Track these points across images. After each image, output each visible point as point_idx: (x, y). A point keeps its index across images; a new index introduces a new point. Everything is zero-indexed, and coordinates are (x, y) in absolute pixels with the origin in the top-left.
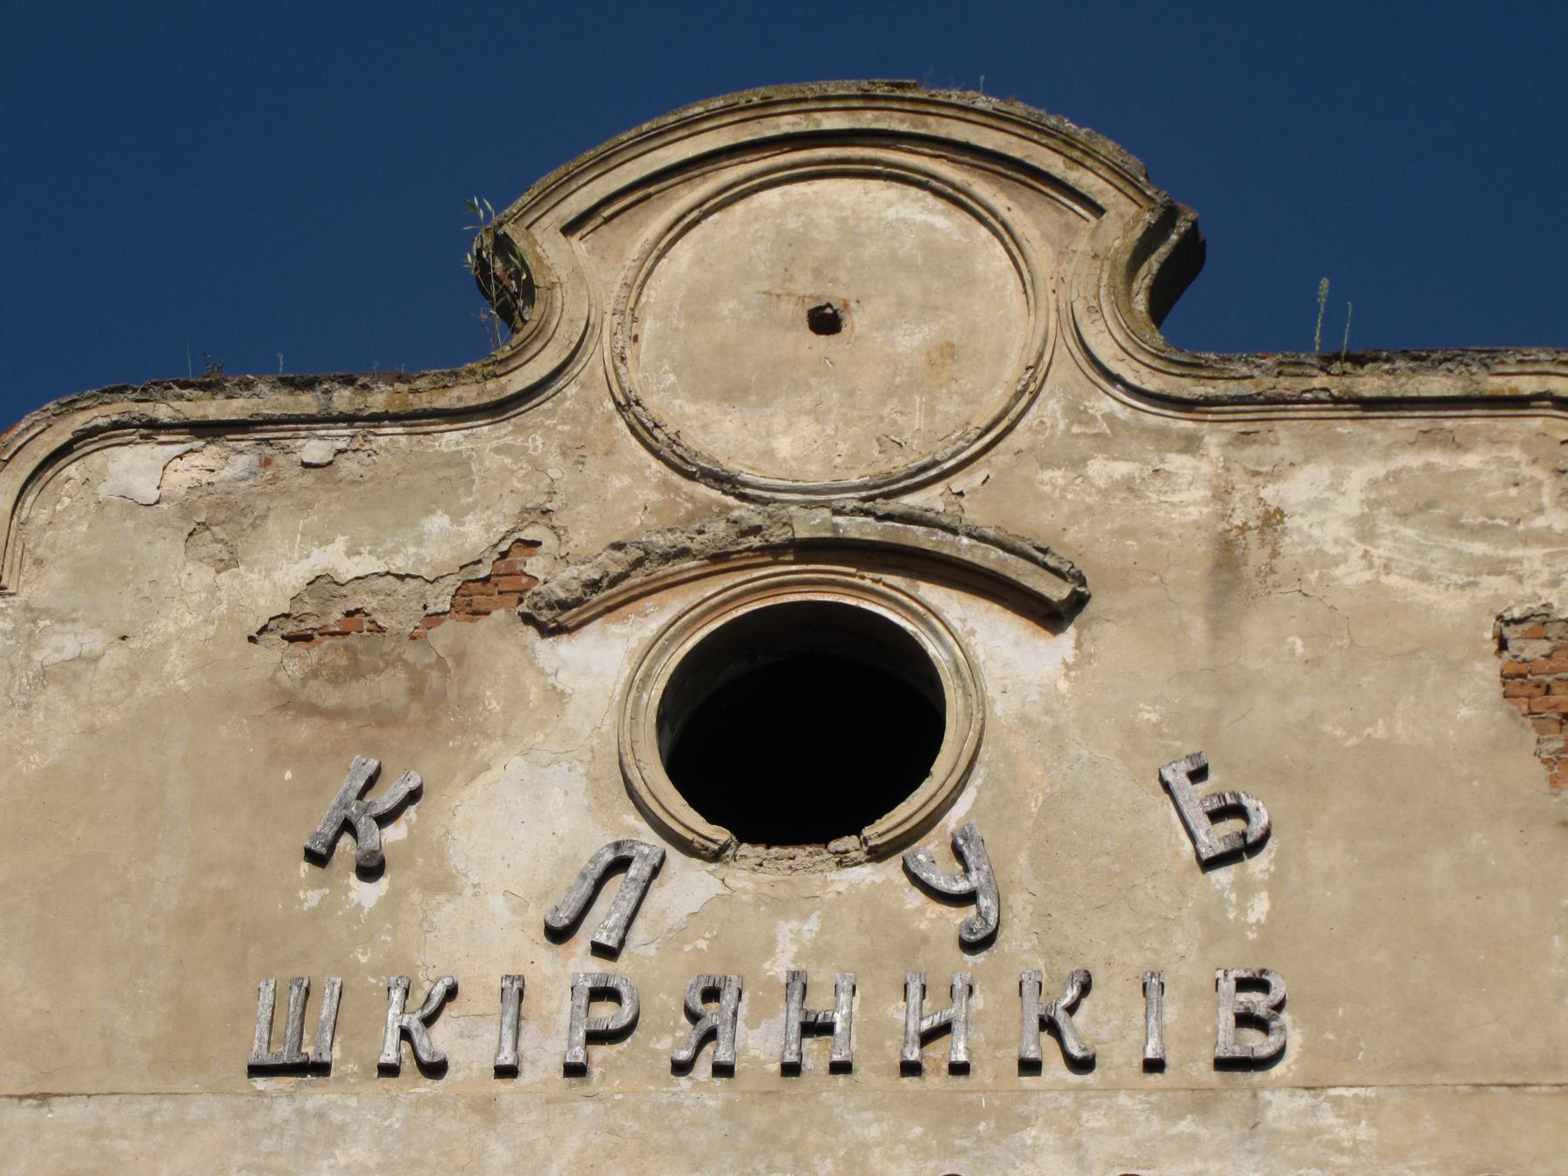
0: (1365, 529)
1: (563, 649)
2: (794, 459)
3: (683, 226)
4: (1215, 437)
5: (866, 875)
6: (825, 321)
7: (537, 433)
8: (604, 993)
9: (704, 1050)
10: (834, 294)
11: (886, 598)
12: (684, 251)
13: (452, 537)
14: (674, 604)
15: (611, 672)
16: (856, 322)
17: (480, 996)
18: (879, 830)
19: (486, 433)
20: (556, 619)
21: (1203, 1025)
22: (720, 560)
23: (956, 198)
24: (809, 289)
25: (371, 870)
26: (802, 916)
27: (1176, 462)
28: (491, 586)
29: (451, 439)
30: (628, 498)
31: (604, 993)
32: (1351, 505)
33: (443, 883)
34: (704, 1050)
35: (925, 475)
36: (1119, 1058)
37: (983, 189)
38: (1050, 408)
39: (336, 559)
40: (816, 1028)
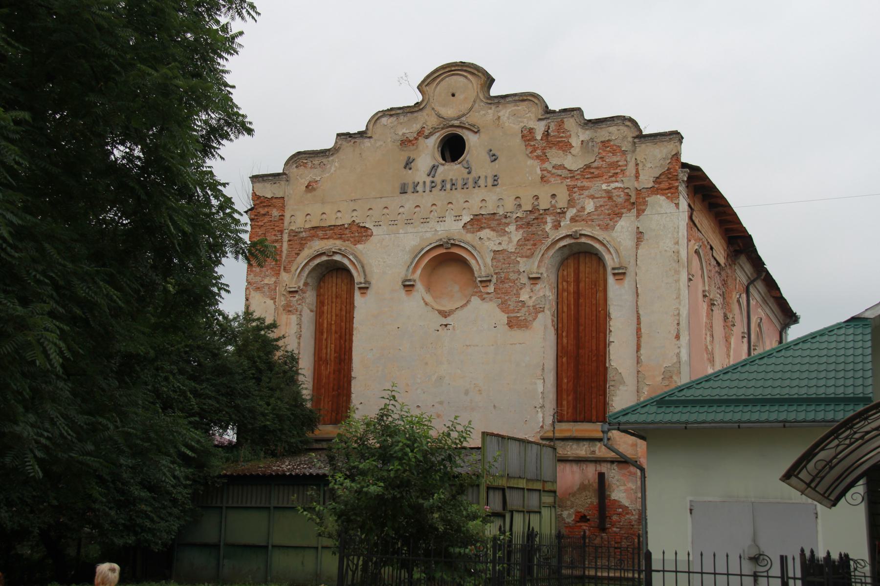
0: (508, 118)
1: (427, 141)
2: (86, 424)
3: (438, 84)
4: (493, 107)
5: (459, 166)
6: (453, 95)
7: (424, 113)
8: (433, 182)
9: (443, 188)
10: (450, 94)
11: (460, 132)
12: (439, 87)
13: (416, 127)
14: (438, 134)
15: (432, 143)
16: (456, 95)
17: (421, 184)
18: (459, 160)
19: (420, 113)
20: (427, 137)
21: (490, 181)
22: (443, 129)
23: (466, 77)
24: (452, 91)
25: (410, 169)
26: (452, 171)
27: (489, 111)
28: (420, 133)
29: (415, 114)
30: (433, 121)
31: (433, 182)
32: (507, 115)
33: (417, 170)
34: (443, 188)
35: (464, 115)
36: (483, 185)
37: (469, 76)
38: (476, 105)
39: (404, 131)
40: (453, 184)
